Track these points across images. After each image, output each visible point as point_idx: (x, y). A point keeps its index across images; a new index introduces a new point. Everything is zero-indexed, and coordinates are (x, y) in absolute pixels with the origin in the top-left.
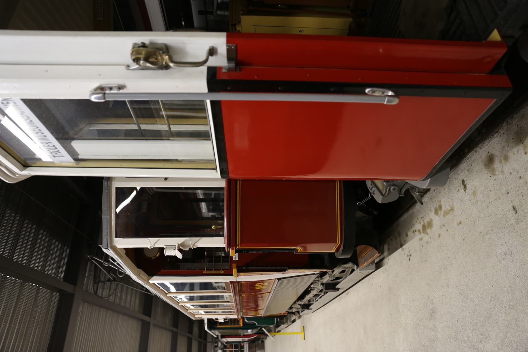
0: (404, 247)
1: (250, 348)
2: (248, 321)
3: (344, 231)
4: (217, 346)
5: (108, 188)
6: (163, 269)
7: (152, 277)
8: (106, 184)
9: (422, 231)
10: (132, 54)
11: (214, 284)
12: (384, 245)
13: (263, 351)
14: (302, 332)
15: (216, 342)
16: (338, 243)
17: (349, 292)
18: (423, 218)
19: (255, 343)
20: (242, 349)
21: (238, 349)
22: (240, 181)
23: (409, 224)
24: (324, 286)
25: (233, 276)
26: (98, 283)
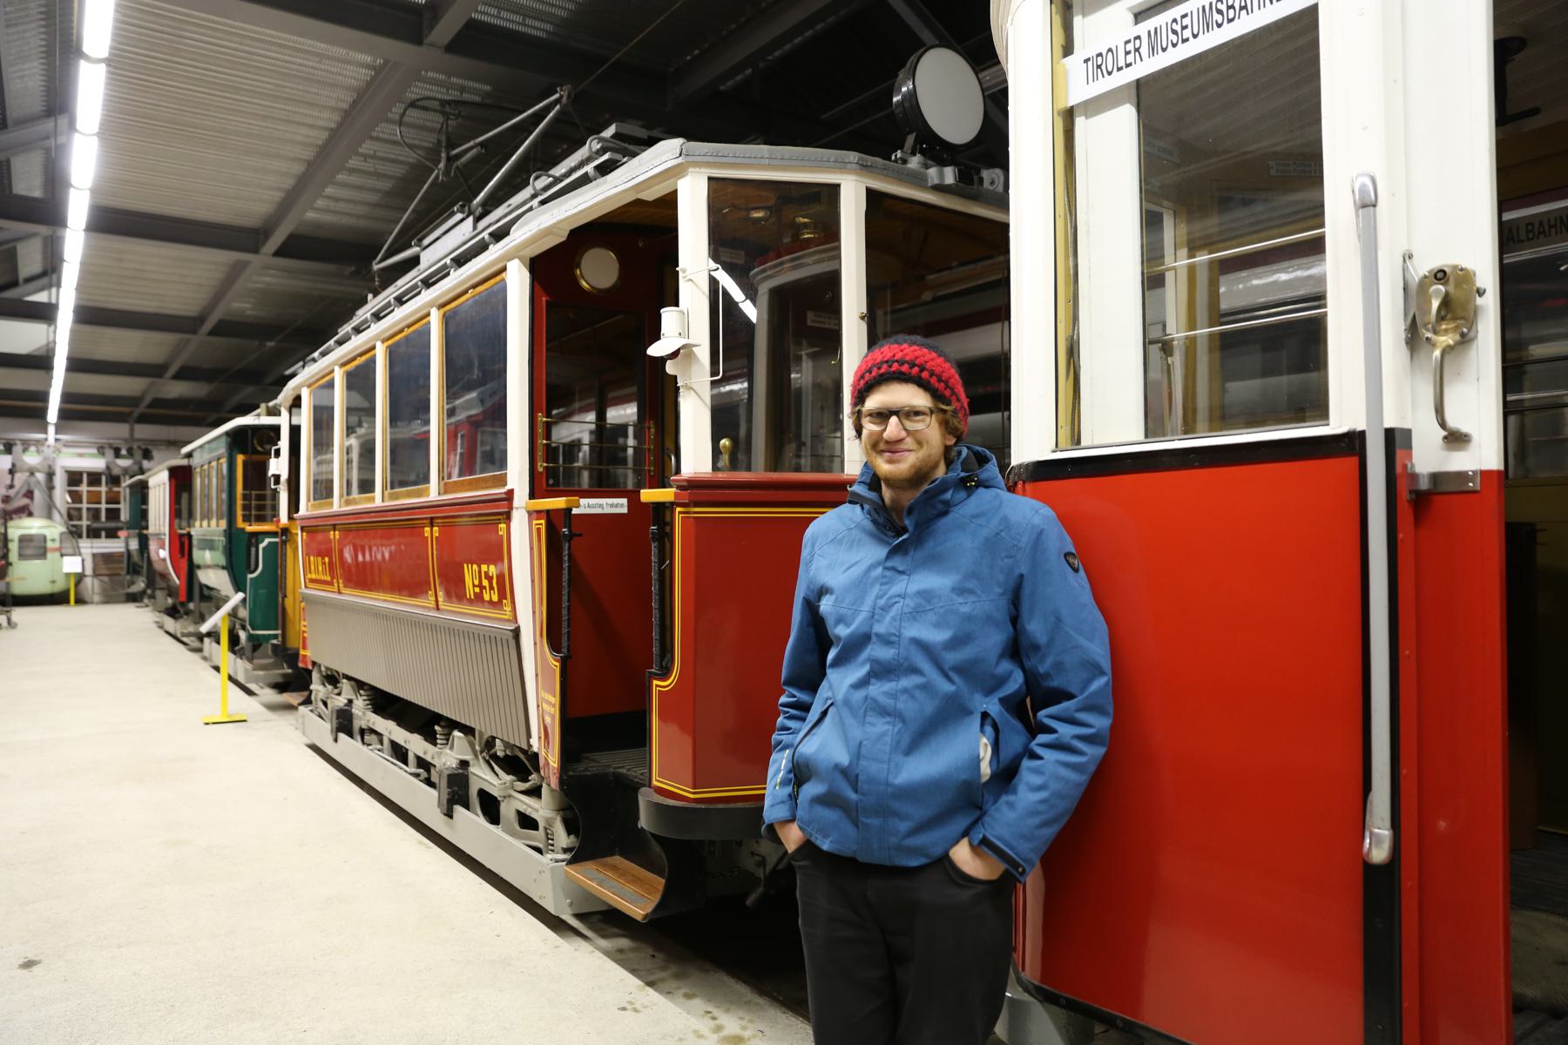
0: (650, 991)
2: (264, 549)
3: (731, 806)
5: (841, 164)
6: (549, 299)
8: (851, 159)
9: (722, 1034)
10: (1455, 267)
11: (274, 448)
12: (623, 936)
14: (229, 716)
18: (760, 1034)
19: (128, 573)
20: (103, 534)
23: (730, 1003)
24: (460, 771)
26: (443, 113)
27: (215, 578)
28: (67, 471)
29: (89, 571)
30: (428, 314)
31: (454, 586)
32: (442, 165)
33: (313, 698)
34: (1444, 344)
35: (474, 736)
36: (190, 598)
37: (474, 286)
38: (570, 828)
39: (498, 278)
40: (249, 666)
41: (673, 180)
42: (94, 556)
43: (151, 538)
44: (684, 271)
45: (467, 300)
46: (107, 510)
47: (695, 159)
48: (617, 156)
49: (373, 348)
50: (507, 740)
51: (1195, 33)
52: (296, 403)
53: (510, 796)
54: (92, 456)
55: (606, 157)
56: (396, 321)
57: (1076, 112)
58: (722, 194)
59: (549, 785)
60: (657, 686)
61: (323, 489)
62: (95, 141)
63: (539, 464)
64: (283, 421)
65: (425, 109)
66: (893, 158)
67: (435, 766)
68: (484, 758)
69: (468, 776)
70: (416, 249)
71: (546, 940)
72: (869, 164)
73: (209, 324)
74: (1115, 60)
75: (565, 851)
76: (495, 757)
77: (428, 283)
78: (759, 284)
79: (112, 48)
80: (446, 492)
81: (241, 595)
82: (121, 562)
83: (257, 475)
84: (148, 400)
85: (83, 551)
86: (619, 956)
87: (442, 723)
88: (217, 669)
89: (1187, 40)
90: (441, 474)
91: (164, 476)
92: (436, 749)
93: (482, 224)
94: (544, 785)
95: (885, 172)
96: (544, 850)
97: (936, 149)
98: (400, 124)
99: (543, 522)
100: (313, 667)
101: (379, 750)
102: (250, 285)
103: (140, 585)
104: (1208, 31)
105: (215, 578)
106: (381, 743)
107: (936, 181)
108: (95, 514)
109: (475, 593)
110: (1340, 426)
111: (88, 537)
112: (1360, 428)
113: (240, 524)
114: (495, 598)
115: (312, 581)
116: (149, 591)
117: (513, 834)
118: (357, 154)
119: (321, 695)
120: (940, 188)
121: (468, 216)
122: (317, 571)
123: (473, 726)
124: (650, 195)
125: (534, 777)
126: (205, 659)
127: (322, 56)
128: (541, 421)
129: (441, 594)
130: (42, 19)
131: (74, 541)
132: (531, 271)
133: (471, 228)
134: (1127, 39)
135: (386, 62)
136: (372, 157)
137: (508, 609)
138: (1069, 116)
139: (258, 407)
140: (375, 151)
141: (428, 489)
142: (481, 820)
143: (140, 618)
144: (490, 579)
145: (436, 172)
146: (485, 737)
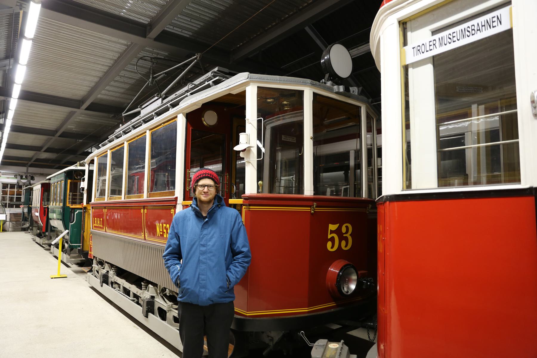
7: (185, 117)
8: (308, 82)
14: (60, 275)
15: (26, 177)
16: (247, 313)
17: (138, 328)
19: (23, 221)
21: (15, 201)
24: (151, 300)
26: (151, 62)
27: (57, 223)
28: (2, 183)
29: (8, 220)
30: (146, 132)
32: (150, 80)
33: (93, 270)
36: (47, 231)
37: (164, 123)
39: (174, 120)
40: (69, 257)
42: (11, 214)
43: (33, 208)
44: (248, 120)
45: (161, 128)
46: (16, 197)
48: (221, 78)
49: (124, 143)
51: (458, 39)
52: (92, 162)
53: (171, 310)
54: (12, 178)
55: (217, 78)
57: (409, 66)
58: (262, 92)
63: (187, 188)
64: (86, 168)
65: (145, 60)
66: (321, 82)
67: (141, 297)
68: (161, 295)
69: (154, 302)
70: (139, 109)
72: (314, 84)
73: (59, 133)
74: (425, 47)
76: (165, 295)
77: (145, 121)
78: (266, 126)
79: (35, 35)
80: (150, 197)
81: (67, 231)
82: (21, 216)
83: (75, 187)
84: (34, 159)
85: (6, 212)
87: (144, 282)
88: (57, 258)
89: (455, 41)
91: (39, 186)
93: (165, 101)
97: (336, 79)
100: (94, 258)
101: (119, 290)
102: (76, 120)
103: (27, 225)
104: (464, 38)
105: (57, 223)
106: (120, 288)
107: (337, 91)
108: (11, 199)
109: (160, 235)
110: (526, 185)
111: (9, 207)
112: (246, 193)
115: (95, 227)
116: (31, 228)
117: (171, 325)
118: (119, 75)
119: (96, 269)
120: (338, 93)
121: (160, 98)
122: (97, 223)
123: (157, 283)
124: (234, 92)
126: (51, 253)
128: (188, 172)
130: (7, 26)
131: (3, 208)
132: (186, 118)
133: (161, 103)
134: (430, 40)
135: (132, 43)
139: (77, 163)
141: (143, 195)
142: (159, 319)
143: (26, 237)
144: (167, 230)
145: (148, 82)
146: (161, 288)
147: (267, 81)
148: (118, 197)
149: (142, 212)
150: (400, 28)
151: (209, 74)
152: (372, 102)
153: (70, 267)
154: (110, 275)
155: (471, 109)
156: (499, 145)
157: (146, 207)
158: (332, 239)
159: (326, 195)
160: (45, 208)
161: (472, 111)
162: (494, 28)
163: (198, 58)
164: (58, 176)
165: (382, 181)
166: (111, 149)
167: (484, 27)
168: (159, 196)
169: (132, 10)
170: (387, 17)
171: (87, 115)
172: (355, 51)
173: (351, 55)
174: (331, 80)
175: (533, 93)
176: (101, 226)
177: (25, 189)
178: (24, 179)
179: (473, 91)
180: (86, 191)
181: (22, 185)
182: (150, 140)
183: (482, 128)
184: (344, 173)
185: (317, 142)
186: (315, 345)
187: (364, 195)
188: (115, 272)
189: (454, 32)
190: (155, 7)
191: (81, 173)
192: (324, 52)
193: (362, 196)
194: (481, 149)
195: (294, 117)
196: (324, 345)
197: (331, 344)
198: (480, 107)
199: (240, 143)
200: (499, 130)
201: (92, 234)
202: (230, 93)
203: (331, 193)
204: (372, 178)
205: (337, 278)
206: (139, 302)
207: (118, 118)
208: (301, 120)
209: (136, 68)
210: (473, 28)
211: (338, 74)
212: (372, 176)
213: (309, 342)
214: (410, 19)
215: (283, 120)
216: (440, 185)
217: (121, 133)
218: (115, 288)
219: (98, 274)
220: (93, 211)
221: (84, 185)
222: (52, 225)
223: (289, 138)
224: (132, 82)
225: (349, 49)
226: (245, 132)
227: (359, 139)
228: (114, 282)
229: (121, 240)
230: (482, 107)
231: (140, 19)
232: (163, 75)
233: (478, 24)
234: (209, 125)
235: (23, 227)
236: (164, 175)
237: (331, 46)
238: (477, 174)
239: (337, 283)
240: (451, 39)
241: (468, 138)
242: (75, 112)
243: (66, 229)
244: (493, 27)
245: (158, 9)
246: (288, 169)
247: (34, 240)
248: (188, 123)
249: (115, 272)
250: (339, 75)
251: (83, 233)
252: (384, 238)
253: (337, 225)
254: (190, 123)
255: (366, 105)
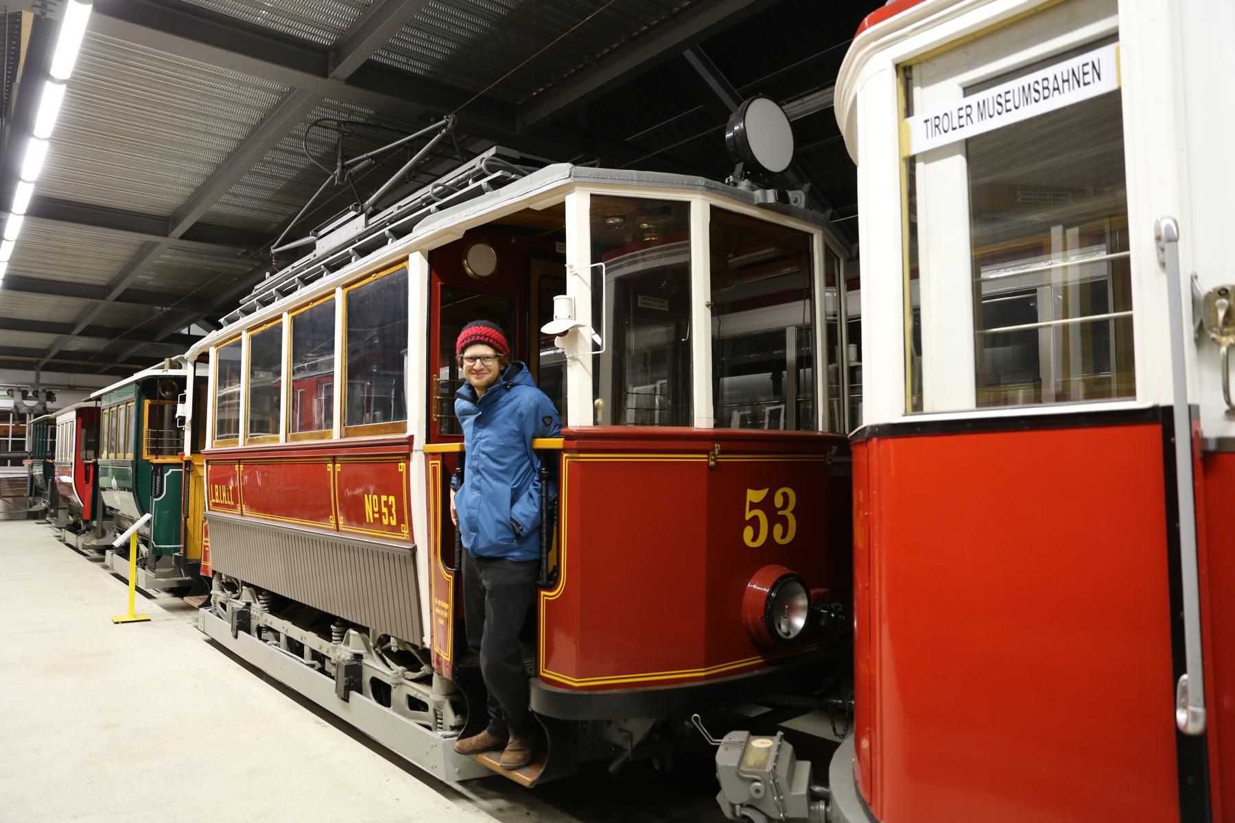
1: (13, 482)
3: (608, 692)
4: (25, 395)
8: (700, 182)
13: (1, 516)
15: (36, 395)
19: (31, 495)
21: (10, 450)
22: (823, 460)
24: (355, 663)
25: (427, 443)
26: (340, 131)
27: (119, 499)
30: (334, 292)
31: (355, 512)
32: (337, 171)
33: (212, 601)
34: (1228, 343)
35: (369, 636)
36: (94, 517)
37: (377, 272)
38: (457, 709)
39: (400, 266)
40: (151, 574)
41: (562, 195)
44: (571, 267)
46: (12, 441)
47: (581, 179)
48: (507, 174)
49: (280, 317)
50: (401, 638)
51: (1017, 105)
52: (203, 358)
53: (401, 683)
55: (498, 174)
56: (303, 297)
57: (917, 159)
58: (600, 206)
59: (440, 674)
60: (544, 596)
61: (226, 427)
62: (46, 145)
64: (188, 371)
65: (325, 127)
66: (727, 181)
67: (330, 659)
68: (377, 652)
70: (310, 239)
71: (438, 802)
72: (713, 187)
73: (116, 293)
75: (453, 728)
76: (388, 652)
77: (333, 268)
79: (74, 73)
80: (346, 437)
81: (147, 516)
82: (25, 485)
84: (54, 353)
86: (501, 815)
87: (337, 623)
89: (1010, 110)
90: (343, 421)
91: (72, 416)
92: (331, 644)
93: (372, 221)
94: (435, 674)
95: (724, 193)
96: (433, 728)
98: (306, 139)
99: (439, 462)
100: (213, 576)
103: (42, 505)
105: (119, 499)
106: (278, 639)
107: (761, 201)
112: (569, 425)
113: (146, 456)
114: (394, 522)
115: (215, 504)
120: (763, 206)
121: (360, 214)
122: (220, 497)
123: (369, 626)
124: (539, 206)
125: (425, 669)
126: (106, 567)
127: (240, 83)
128: (436, 381)
129: (341, 518)
132: (429, 261)
134: (960, 107)
135: (292, 89)
136: (269, 163)
137: (406, 532)
138: (911, 162)
139: (164, 360)
140: (273, 159)
142: (373, 702)
143: (41, 533)
146: (378, 636)
147: (610, 181)
148: (269, 438)
149: (328, 470)
150: (899, 79)
151: (477, 163)
152: (833, 217)
153: (154, 598)
154: (255, 613)
155: (1049, 236)
156: (1106, 321)
157: (339, 459)
158: (755, 522)
159: (729, 426)
160: (89, 464)
161: (1050, 240)
162: (1087, 86)
163: (450, 125)
164: (120, 391)
165: (862, 394)
166: (250, 330)
167: (1066, 84)
168: (368, 433)
169: (281, 10)
170: (872, 56)
171: (189, 251)
172: (798, 105)
173: (788, 115)
174: (746, 177)
175: (1158, 222)
176: (229, 503)
177: (33, 422)
178: (30, 399)
179: (1052, 200)
180: (190, 425)
181: (26, 412)
182: (345, 311)
183: (1074, 278)
184: (772, 378)
185: (718, 308)
186: (722, 743)
187: (821, 426)
188: (265, 605)
189: (1009, 92)
190: (352, 10)
191: (174, 383)
192: (733, 114)
193: (815, 429)
194: (1071, 329)
195: (667, 256)
196: (741, 742)
197: (755, 739)
198: (1069, 231)
199: (556, 317)
200: (1106, 281)
201: (209, 522)
202: (528, 208)
203: (741, 421)
204: (838, 388)
205: (767, 605)
206: (326, 669)
207: (255, 257)
208: (684, 263)
209: (305, 144)
210: (1045, 84)
211: (761, 163)
212: (837, 383)
213: (711, 737)
214: (918, 60)
215: (644, 261)
216: (980, 403)
217: (274, 292)
218: (268, 641)
219: (225, 610)
220: (210, 469)
221: (185, 410)
222: (108, 503)
223: (653, 303)
224: (290, 174)
225: (782, 102)
226: (565, 294)
227: (808, 301)
228: (264, 626)
229: (280, 532)
230: (1074, 232)
231: (316, 35)
232: (366, 161)
233: (1055, 78)
234: (478, 276)
235: (31, 510)
236: (362, 386)
237: (746, 102)
238: (1061, 376)
239: (765, 614)
240: (1002, 105)
241: (1047, 304)
242: (154, 245)
243: (143, 510)
244: (1085, 84)
245: (356, 13)
246: (649, 368)
247: (62, 538)
248: (433, 272)
249: (265, 605)
250: (765, 166)
251: (186, 520)
252: (868, 512)
253: (765, 492)
254: (436, 272)
255: (824, 230)
